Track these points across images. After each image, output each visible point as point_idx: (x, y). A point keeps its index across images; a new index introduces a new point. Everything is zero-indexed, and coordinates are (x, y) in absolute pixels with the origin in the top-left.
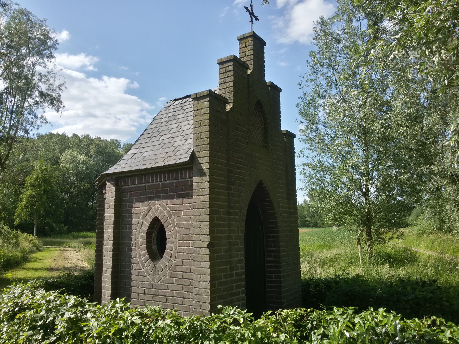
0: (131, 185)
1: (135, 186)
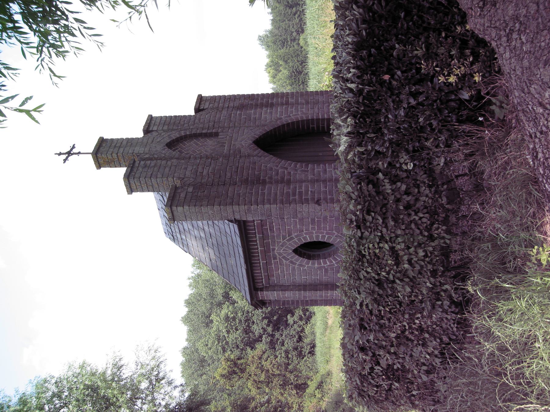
0: (262, 276)
1: (262, 272)
